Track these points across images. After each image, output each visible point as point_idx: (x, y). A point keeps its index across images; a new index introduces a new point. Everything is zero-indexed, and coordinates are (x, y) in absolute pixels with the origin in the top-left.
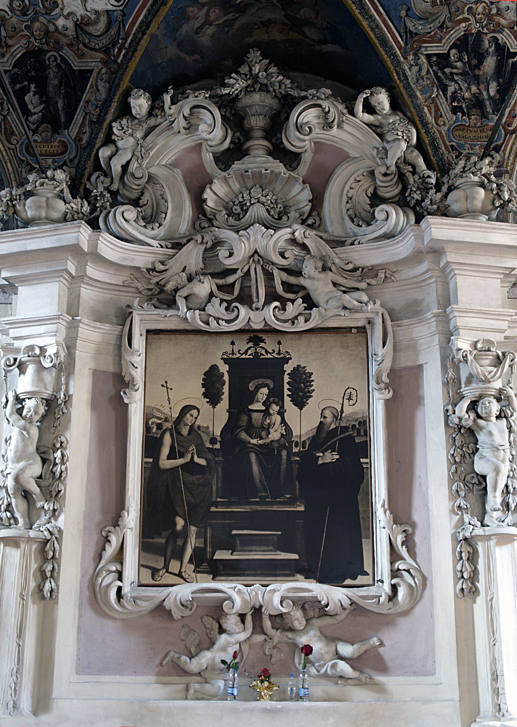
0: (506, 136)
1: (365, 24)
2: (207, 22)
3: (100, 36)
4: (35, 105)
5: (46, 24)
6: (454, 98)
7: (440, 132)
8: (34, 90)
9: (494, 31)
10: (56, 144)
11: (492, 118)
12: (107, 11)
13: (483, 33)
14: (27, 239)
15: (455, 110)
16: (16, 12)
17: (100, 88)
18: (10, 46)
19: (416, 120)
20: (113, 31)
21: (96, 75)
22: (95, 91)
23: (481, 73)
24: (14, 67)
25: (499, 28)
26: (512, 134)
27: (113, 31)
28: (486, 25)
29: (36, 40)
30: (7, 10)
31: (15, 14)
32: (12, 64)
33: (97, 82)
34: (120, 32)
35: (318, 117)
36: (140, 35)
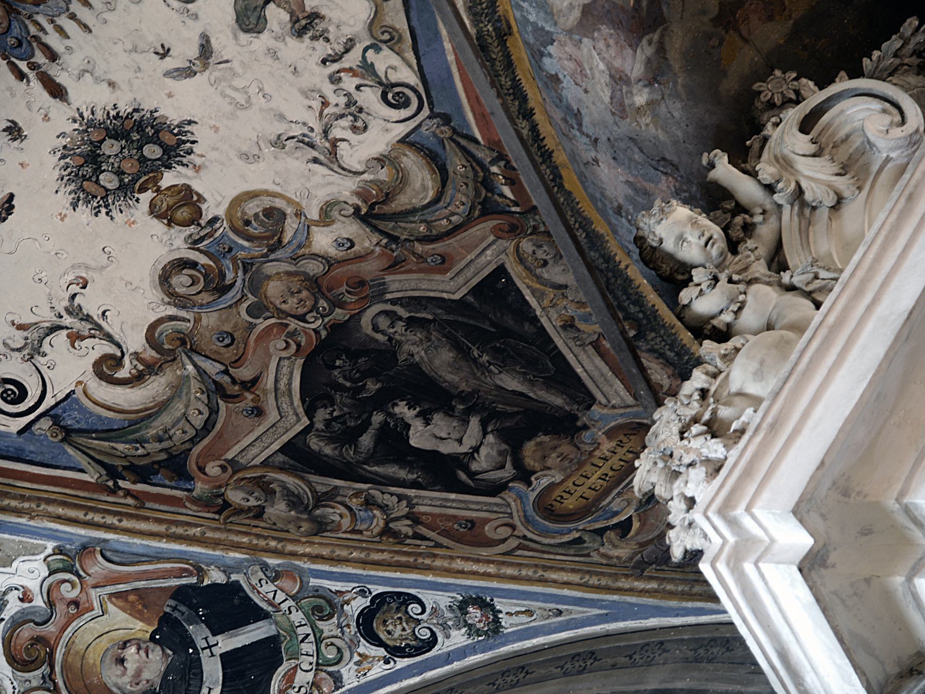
3: (436, 200)
4: (456, 435)
5: (292, 268)
8: (413, 413)
10: (607, 446)
12: (402, 141)
14: (870, 308)
16: (198, 299)
17: (560, 280)
18: (255, 381)
20: (457, 165)
21: (520, 268)
24: (310, 413)
27: (457, 165)
29: (302, 318)
30: (172, 311)
31: (201, 306)
32: (301, 410)
33: (539, 278)
34: (473, 156)
36: (524, 125)
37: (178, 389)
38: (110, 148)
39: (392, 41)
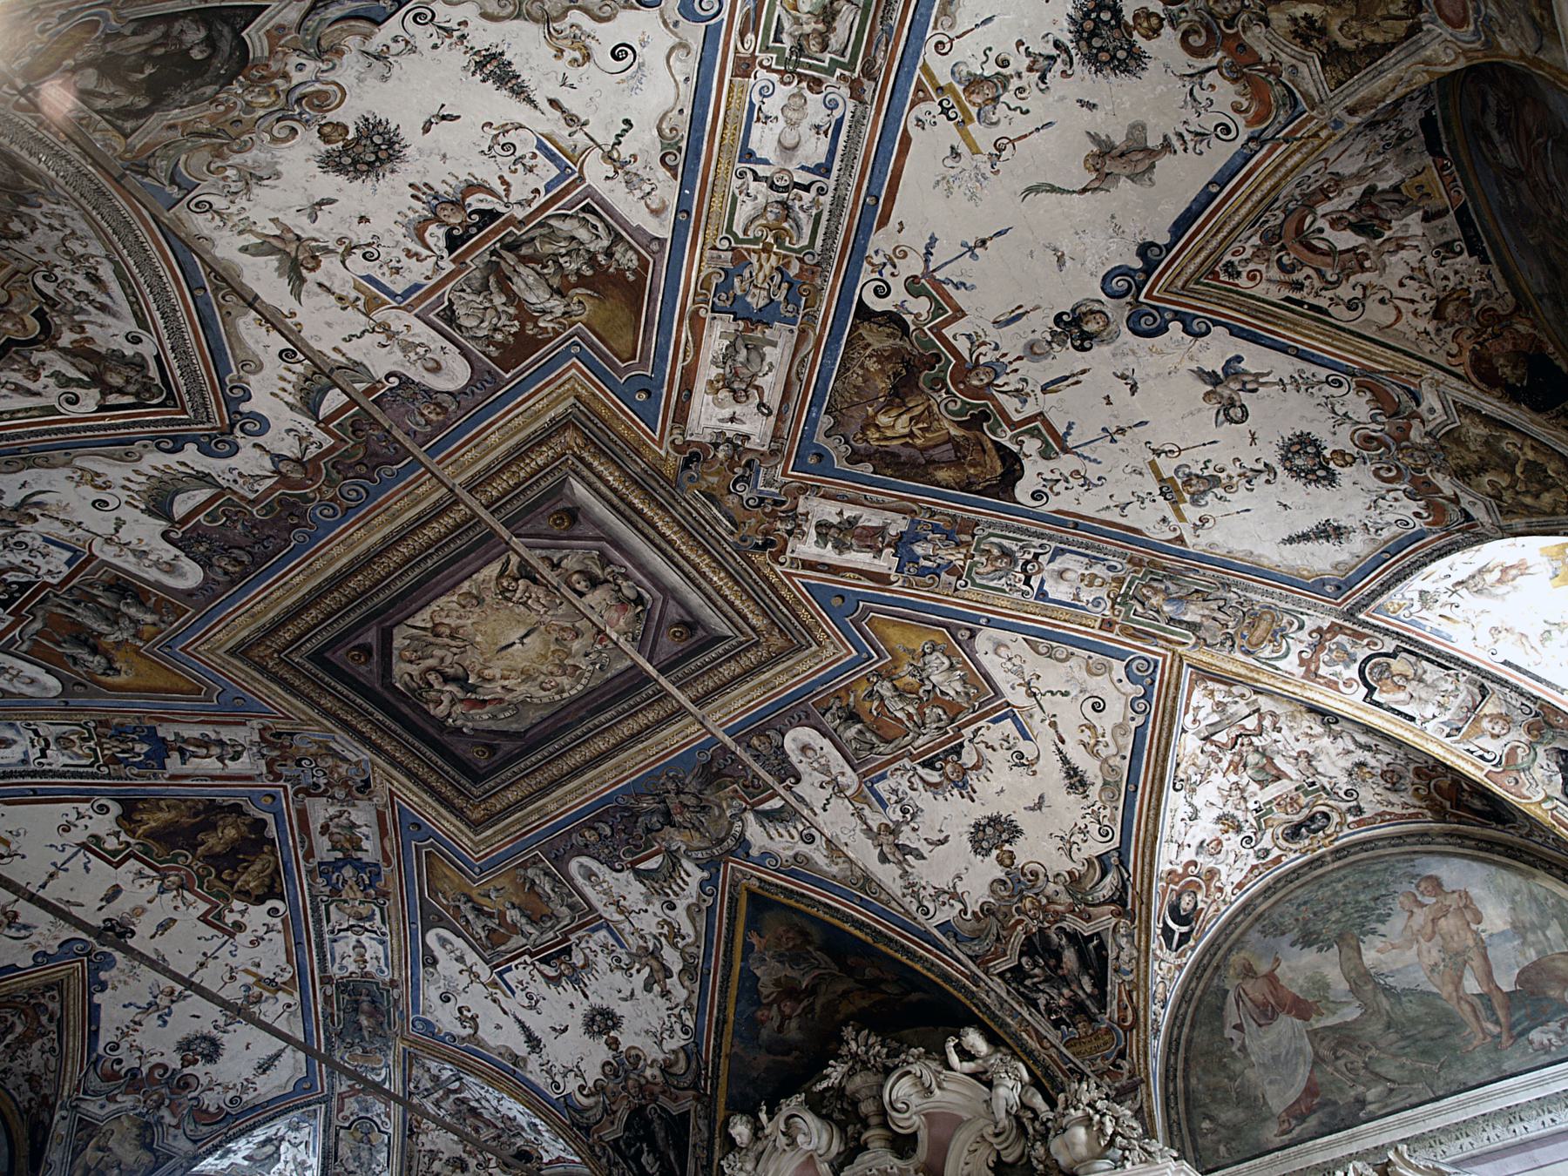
1: (918, 967)
2: (785, 1018)
6: (1049, 1011)
7: (1050, 1056)
15: (1056, 1025)
19: (1020, 1052)
20: (694, 1065)
22: (697, 1133)
25: (1060, 917)
27: (694, 1065)
35: (915, 1085)
37: (597, 1103)
38: (598, 1018)
39: (691, 1010)
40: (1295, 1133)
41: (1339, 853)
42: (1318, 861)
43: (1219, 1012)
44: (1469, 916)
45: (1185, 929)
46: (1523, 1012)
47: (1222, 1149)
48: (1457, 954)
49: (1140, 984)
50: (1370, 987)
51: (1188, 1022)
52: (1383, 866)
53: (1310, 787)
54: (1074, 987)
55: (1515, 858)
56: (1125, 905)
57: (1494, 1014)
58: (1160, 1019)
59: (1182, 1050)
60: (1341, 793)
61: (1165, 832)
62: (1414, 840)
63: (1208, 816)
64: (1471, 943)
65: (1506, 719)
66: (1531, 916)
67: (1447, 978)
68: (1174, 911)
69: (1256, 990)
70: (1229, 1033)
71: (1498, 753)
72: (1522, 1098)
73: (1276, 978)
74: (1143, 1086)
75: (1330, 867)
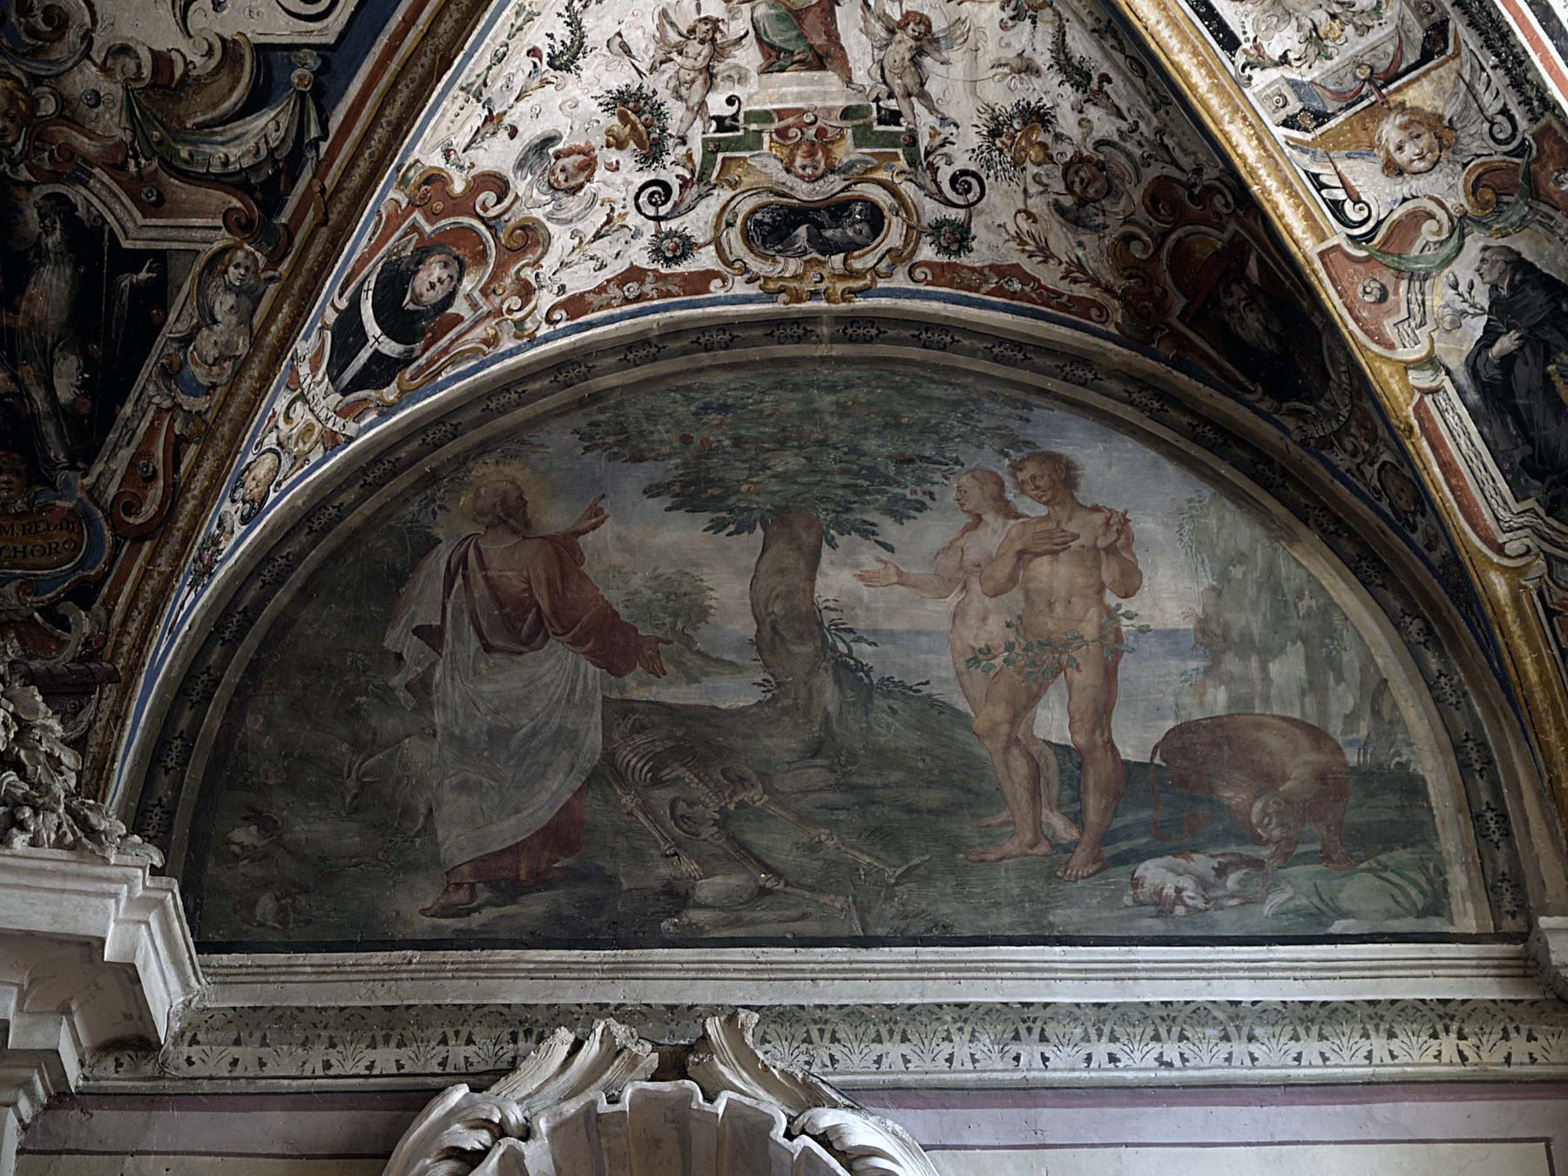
0: (117, 546)
9: (57, 178)
11: (67, 483)
13: (18, 184)
23: (21, 321)
25: (74, 168)
26: (138, 540)
28: (25, 155)
40: (476, 920)
41: (854, 326)
42: (798, 327)
43: (390, 583)
44: (1109, 572)
45: (391, 348)
46: (1145, 814)
47: (266, 904)
48: (1048, 644)
49: (223, 429)
50: (807, 649)
51: (297, 579)
52: (956, 394)
53: (878, 125)
54: (27, 372)
55: (1267, 487)
56: (272, 204)
57: (1078, 798)
58: (226, 545)
59: (251, 642)
60: (945, 175)
61: (474, 64)
62: (1050, 363)
63: (602, 74)
64: (1089, 630)
65: (1440, 134)
66: (1248, 619)
67: (1002, 688)
68: (394, 281)
69: (511, 564)
70: (398, 638)
71: (1379, 212)
72: (1065, 994)
73: (576, 556)
74: (110, 692)
75: (821, 351)
